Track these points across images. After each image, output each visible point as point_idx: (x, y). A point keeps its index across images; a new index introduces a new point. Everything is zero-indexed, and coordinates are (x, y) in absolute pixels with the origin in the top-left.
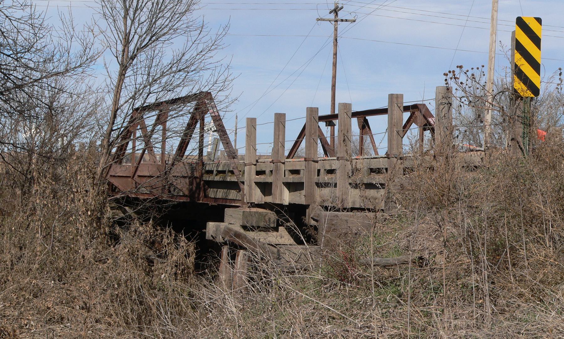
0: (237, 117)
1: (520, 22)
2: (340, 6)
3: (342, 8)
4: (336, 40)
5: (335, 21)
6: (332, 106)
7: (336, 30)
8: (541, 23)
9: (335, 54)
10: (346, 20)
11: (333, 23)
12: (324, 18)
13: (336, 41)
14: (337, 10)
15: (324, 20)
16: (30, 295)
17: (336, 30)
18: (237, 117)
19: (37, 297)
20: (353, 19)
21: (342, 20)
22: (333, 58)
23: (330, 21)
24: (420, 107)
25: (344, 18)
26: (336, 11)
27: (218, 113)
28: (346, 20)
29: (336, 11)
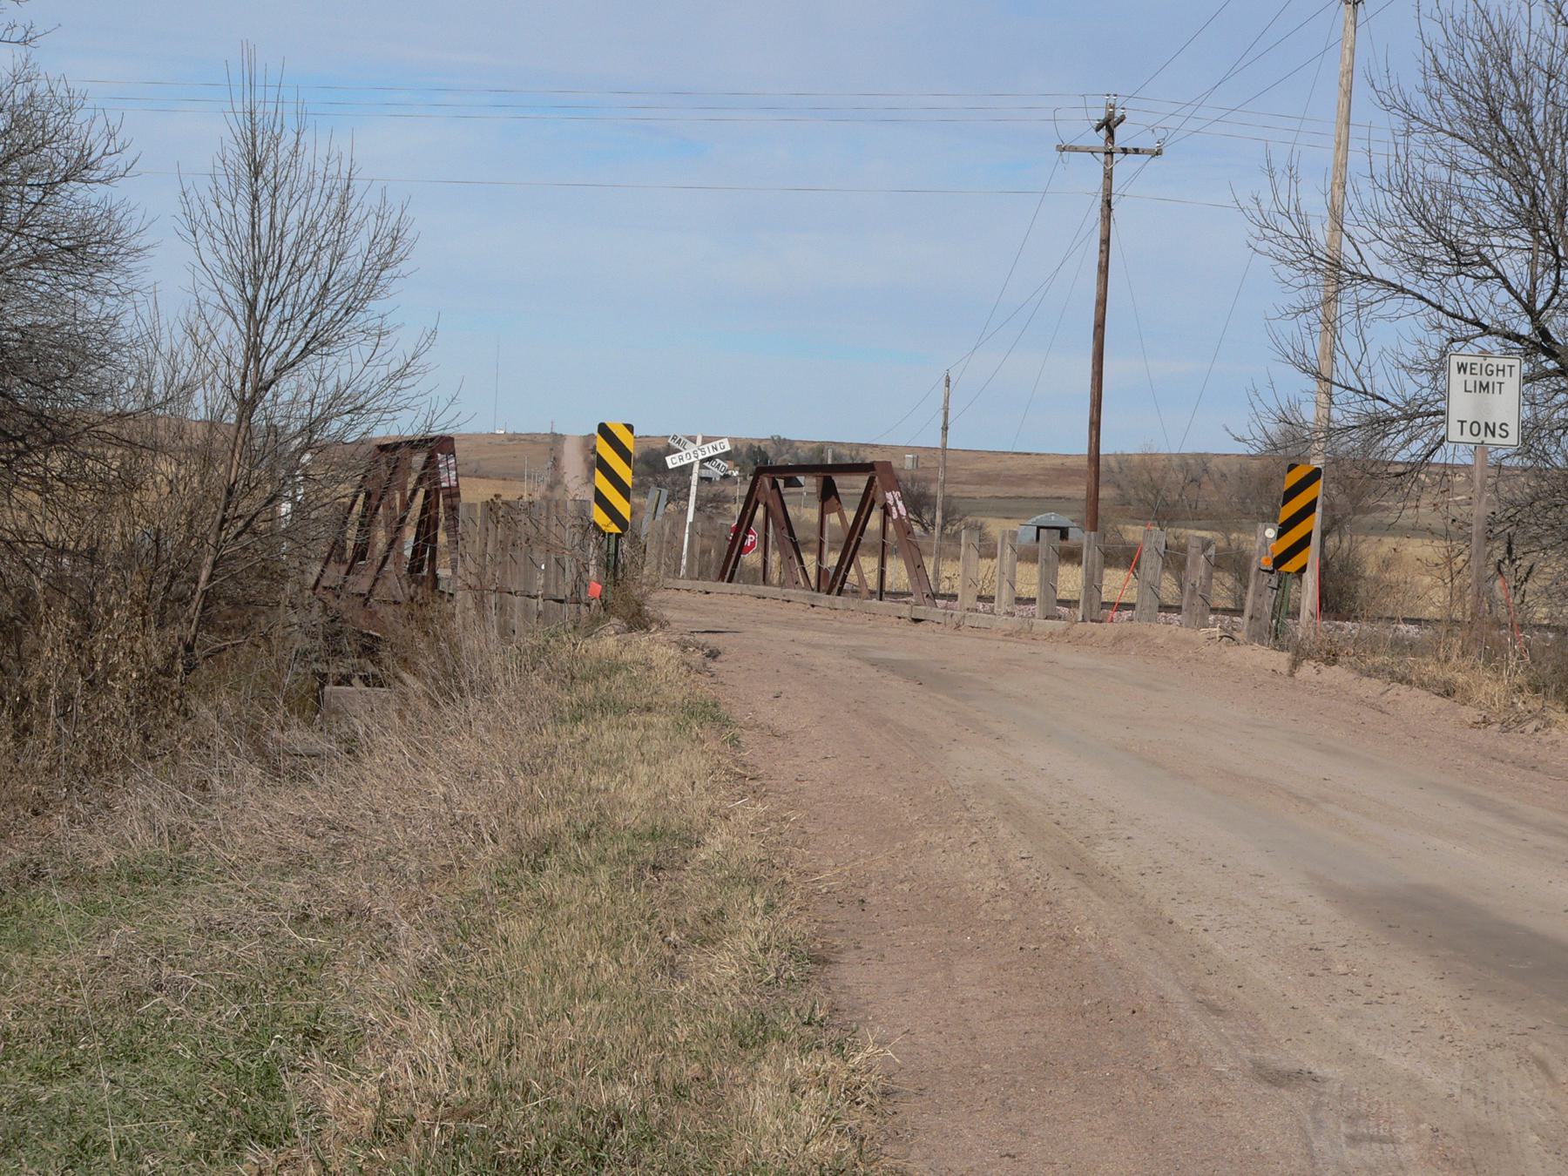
0: (948, 380)
1: (604, 430)
2: (1118, 114)
3: (1122, 119)
4: (1109, 203)
5: (1106, 153)
6: (1093, 379)
7: (1108, 176)
8: (632, 431)
9: (1106, 242)
10: (1136, 151)
11: (1102, 157)
12: (1075, 144)
13: (1109, 206)
14: (1111, 124)
15: (1076, 149)
16: (27, 811)
17: (1108, 176)
18: (948, 380)
19: (37, 815)
20: (1155, 146)
21: (1125, 151)
22: (1098, 251)
23: (1092, 152)
24: (876, 467)
25: (1129, 146)
26: (1109, 125)
27: (457, 480)
28: (1136, 151)
29: (1109, 125)
